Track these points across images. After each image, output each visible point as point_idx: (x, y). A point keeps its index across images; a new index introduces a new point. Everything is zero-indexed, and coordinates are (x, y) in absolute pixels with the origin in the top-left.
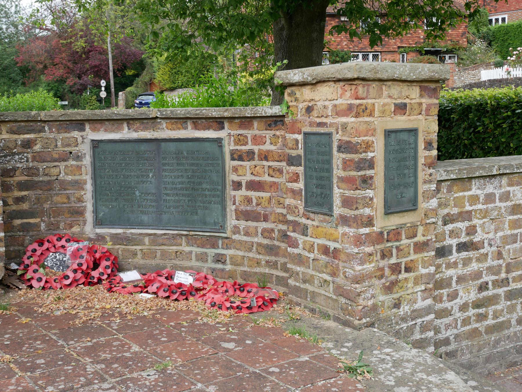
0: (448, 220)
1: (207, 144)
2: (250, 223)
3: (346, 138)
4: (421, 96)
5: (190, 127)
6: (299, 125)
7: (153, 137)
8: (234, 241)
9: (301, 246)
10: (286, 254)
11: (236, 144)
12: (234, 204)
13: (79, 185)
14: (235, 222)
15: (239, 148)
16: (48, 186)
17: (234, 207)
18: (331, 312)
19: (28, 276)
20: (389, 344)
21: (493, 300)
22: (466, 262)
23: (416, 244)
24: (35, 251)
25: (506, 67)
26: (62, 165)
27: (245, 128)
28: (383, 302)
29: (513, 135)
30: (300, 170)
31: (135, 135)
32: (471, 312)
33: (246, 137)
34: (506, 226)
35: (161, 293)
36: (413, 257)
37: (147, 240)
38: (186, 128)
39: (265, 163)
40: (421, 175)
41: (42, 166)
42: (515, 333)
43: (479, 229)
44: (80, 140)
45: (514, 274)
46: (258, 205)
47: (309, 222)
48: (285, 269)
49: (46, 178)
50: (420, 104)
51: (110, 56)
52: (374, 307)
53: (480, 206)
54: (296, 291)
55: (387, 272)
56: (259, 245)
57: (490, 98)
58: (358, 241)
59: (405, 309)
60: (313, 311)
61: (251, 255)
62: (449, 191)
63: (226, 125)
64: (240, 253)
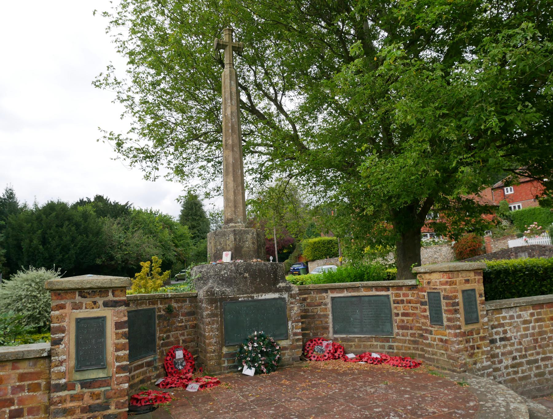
0: (493, 327)
2: (404, 331)
3: (446, 294)
4: (475, 276)
6: (425, 289)
8: (397, 339)
9: (430, 339)
10: (423, 344)
11: (395, 297)
13: (326, 316)
14: (397, 331)
15: (397, 298)
16: (313, 317)
17: (396, 324)
18: (446, 367)
19: (310, 355)
20: (474, 378)
21: (520, 365)
22: (505, 346)
23: (480, 337)
24: (309, 345)
25: (524, 237)
26: (319, 308)
27: (399, 290)
28: (469, 362)
29: (525, 286)
30: (427, 307)
31: (350, 294)
32: (510, 370)
34: (522, 330)
35: (369, 361)
36: (479, 343)
37: (356, 340)
38: (372, 291)
39: (409, 305)
40: (480, 307)
41: (311, 308)
42: (534, 381)
43: (509, 331)
44: (326, 297)
45: (529, 352)
46: (407, 323)
47: (433, 329)
48: (422, 350)
49: (312, 314)
50: (475, 279)
51: (275, 242)
52: (465, 364)
53: (508, 321)
54: (429, 359)
55: (469, 349)
56: (409, 340)
57: (511, 266)
58: (456, 335)
59: (479, 365)
60: (438, 367)
61: (406, 345)
62: (492, 314)
63: (390, 289)
64: (401, 344)
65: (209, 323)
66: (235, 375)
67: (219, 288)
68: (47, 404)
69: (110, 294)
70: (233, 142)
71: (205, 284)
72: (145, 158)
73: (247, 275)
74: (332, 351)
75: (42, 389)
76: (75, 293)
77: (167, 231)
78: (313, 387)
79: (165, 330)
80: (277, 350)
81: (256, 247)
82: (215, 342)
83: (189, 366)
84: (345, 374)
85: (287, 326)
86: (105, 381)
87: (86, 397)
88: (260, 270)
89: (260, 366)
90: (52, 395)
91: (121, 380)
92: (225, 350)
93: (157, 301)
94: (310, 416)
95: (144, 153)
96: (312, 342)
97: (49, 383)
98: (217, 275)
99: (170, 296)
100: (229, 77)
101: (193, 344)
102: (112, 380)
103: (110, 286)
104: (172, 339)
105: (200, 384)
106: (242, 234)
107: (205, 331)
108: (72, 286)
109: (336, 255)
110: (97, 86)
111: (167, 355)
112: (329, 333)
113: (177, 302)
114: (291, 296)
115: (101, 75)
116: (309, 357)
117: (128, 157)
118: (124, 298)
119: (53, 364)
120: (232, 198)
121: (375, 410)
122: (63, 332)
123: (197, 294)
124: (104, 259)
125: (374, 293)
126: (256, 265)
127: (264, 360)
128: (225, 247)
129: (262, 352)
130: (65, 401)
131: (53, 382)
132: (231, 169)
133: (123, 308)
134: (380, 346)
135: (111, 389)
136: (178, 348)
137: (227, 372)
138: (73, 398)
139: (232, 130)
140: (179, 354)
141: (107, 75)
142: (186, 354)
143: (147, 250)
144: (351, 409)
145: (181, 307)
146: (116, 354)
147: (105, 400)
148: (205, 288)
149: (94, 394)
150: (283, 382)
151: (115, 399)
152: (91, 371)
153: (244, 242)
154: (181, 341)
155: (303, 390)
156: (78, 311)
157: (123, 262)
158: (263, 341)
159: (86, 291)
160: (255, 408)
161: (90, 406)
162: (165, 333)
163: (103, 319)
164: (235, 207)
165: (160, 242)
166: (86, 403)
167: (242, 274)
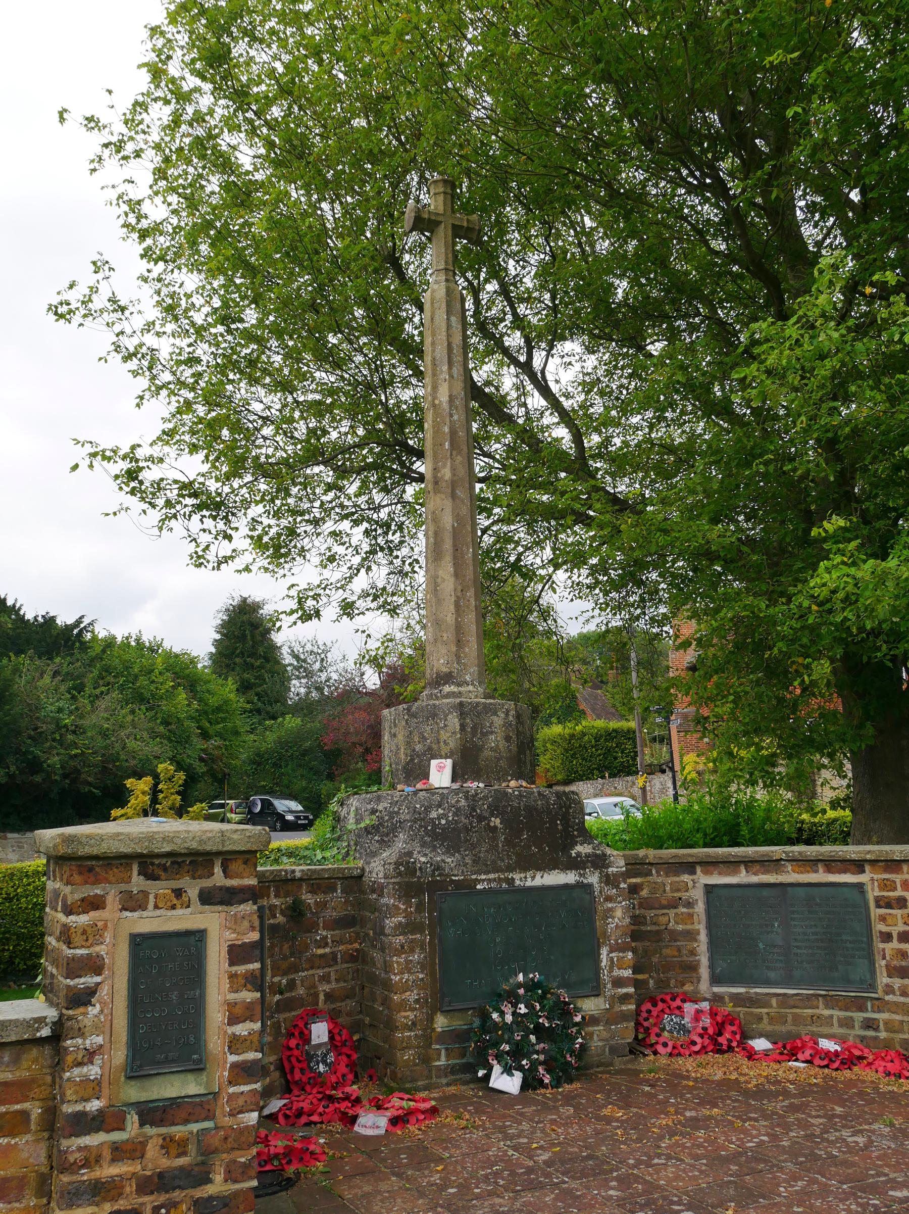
1: (845, 889)
5: (821, 870)
7: (778, 882)
8: (888, 1003)
12: (884, 958)
13: (691, 936)
14: (886, 980)
15: (886, 894)
16: (657, 936)
17: (884, 963)
24: (649, 1012)
26: (672, 913)
31: (754, 879)
33: (895, 882)
35: (817, 1061)
37: (774, 1001)
38: (816, 871)
44: (690, 884)
49: (654, 928)
63: (867, 868)
65: (402, 950)
66: (468, 1091)
67: (425, 855)
68: (44, 1169)
69: (218, 870)
70: (454, 475)
71: (385, 843)
72: (199, 508)
73: (496, 822)
74: (711, 1031)
75: (33, 1127)
76: (129, 867)
77: (182, 696)
78: (697, 1129)
79: (285, 965)
80: (577, 1024)
81: (514, 748)
82: (417, 1001)
83: (343, 1065)
84: (760, 1093)
85: (598, 960)
86: (201, 1104)
87: (152, 1150)
88: (530, 809)
89: (534, 1064)
90: (65, 1143)
91: (241, 1101)
92: (441, 1022)
93: (269, 887)
94: (723, 1205)
95: (195, 495)
96: (655, 1004)
97: (51, 1113)
98: (420, 819)
99: (298, 875)
100: (444, 305)
101: (350, 1004)
102: (219, 1103)
103: (220, 848)
104: (301, 991)
105: (388, 1114)
106: (479, 714)
107: (387, 967)
108: (125, 849)
109: (629, 770)
110: (61, 316)
111: (290, 1035)
112: (699, 981)
113: (313, 891)
114: (609, 880)
115: (71, 287)
116: (652, 1045)
117: (154, 506)
118: (253, 882)
119: (70, 1059)
120: (450, 618)
121: (891, 1193)
122: (98, 971)
123: (363, 869)
124: (13, 768)
125: (821, 876)
126: (520, 795)
127: (543, 1051)
128: (435, 746)
129: (539, 1030)
130: (98, 1160)
131: (68, 1109)
132: (448, 545)
133: (248, 908)
134: (839, 1019)
135: (216, 1128)
136: (315, 1015)
137: (444, 1081)
138: (119, 1152)
139: (451, 444)
140: (320, 1032)
141: (91, 288)
142: (336, 1031)
143: (131, 744)
144: (825, 1189)
145: (323, 905)
146: (231, 1030)
147: (199, 1158)
148: (389, 855)
149: (172, 1139)
150: (606, 1112)
151: (224, 1156)
152: (168, 1077)
153: (485, 735)
154: (322, 997)
155: (671, 1136)
156: (136, 914)
157: (65, 776)
158: (541, 999)
159: (157, 862)
160: (565, 1182)
161: (161, 1175)
162: (284, 974)
163: (200, 936)
164: (459, 643)
165: (166, 723)
166: (150, 1166)
167: (485, 818)
